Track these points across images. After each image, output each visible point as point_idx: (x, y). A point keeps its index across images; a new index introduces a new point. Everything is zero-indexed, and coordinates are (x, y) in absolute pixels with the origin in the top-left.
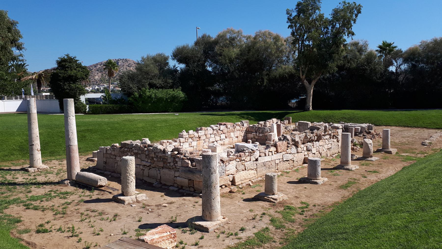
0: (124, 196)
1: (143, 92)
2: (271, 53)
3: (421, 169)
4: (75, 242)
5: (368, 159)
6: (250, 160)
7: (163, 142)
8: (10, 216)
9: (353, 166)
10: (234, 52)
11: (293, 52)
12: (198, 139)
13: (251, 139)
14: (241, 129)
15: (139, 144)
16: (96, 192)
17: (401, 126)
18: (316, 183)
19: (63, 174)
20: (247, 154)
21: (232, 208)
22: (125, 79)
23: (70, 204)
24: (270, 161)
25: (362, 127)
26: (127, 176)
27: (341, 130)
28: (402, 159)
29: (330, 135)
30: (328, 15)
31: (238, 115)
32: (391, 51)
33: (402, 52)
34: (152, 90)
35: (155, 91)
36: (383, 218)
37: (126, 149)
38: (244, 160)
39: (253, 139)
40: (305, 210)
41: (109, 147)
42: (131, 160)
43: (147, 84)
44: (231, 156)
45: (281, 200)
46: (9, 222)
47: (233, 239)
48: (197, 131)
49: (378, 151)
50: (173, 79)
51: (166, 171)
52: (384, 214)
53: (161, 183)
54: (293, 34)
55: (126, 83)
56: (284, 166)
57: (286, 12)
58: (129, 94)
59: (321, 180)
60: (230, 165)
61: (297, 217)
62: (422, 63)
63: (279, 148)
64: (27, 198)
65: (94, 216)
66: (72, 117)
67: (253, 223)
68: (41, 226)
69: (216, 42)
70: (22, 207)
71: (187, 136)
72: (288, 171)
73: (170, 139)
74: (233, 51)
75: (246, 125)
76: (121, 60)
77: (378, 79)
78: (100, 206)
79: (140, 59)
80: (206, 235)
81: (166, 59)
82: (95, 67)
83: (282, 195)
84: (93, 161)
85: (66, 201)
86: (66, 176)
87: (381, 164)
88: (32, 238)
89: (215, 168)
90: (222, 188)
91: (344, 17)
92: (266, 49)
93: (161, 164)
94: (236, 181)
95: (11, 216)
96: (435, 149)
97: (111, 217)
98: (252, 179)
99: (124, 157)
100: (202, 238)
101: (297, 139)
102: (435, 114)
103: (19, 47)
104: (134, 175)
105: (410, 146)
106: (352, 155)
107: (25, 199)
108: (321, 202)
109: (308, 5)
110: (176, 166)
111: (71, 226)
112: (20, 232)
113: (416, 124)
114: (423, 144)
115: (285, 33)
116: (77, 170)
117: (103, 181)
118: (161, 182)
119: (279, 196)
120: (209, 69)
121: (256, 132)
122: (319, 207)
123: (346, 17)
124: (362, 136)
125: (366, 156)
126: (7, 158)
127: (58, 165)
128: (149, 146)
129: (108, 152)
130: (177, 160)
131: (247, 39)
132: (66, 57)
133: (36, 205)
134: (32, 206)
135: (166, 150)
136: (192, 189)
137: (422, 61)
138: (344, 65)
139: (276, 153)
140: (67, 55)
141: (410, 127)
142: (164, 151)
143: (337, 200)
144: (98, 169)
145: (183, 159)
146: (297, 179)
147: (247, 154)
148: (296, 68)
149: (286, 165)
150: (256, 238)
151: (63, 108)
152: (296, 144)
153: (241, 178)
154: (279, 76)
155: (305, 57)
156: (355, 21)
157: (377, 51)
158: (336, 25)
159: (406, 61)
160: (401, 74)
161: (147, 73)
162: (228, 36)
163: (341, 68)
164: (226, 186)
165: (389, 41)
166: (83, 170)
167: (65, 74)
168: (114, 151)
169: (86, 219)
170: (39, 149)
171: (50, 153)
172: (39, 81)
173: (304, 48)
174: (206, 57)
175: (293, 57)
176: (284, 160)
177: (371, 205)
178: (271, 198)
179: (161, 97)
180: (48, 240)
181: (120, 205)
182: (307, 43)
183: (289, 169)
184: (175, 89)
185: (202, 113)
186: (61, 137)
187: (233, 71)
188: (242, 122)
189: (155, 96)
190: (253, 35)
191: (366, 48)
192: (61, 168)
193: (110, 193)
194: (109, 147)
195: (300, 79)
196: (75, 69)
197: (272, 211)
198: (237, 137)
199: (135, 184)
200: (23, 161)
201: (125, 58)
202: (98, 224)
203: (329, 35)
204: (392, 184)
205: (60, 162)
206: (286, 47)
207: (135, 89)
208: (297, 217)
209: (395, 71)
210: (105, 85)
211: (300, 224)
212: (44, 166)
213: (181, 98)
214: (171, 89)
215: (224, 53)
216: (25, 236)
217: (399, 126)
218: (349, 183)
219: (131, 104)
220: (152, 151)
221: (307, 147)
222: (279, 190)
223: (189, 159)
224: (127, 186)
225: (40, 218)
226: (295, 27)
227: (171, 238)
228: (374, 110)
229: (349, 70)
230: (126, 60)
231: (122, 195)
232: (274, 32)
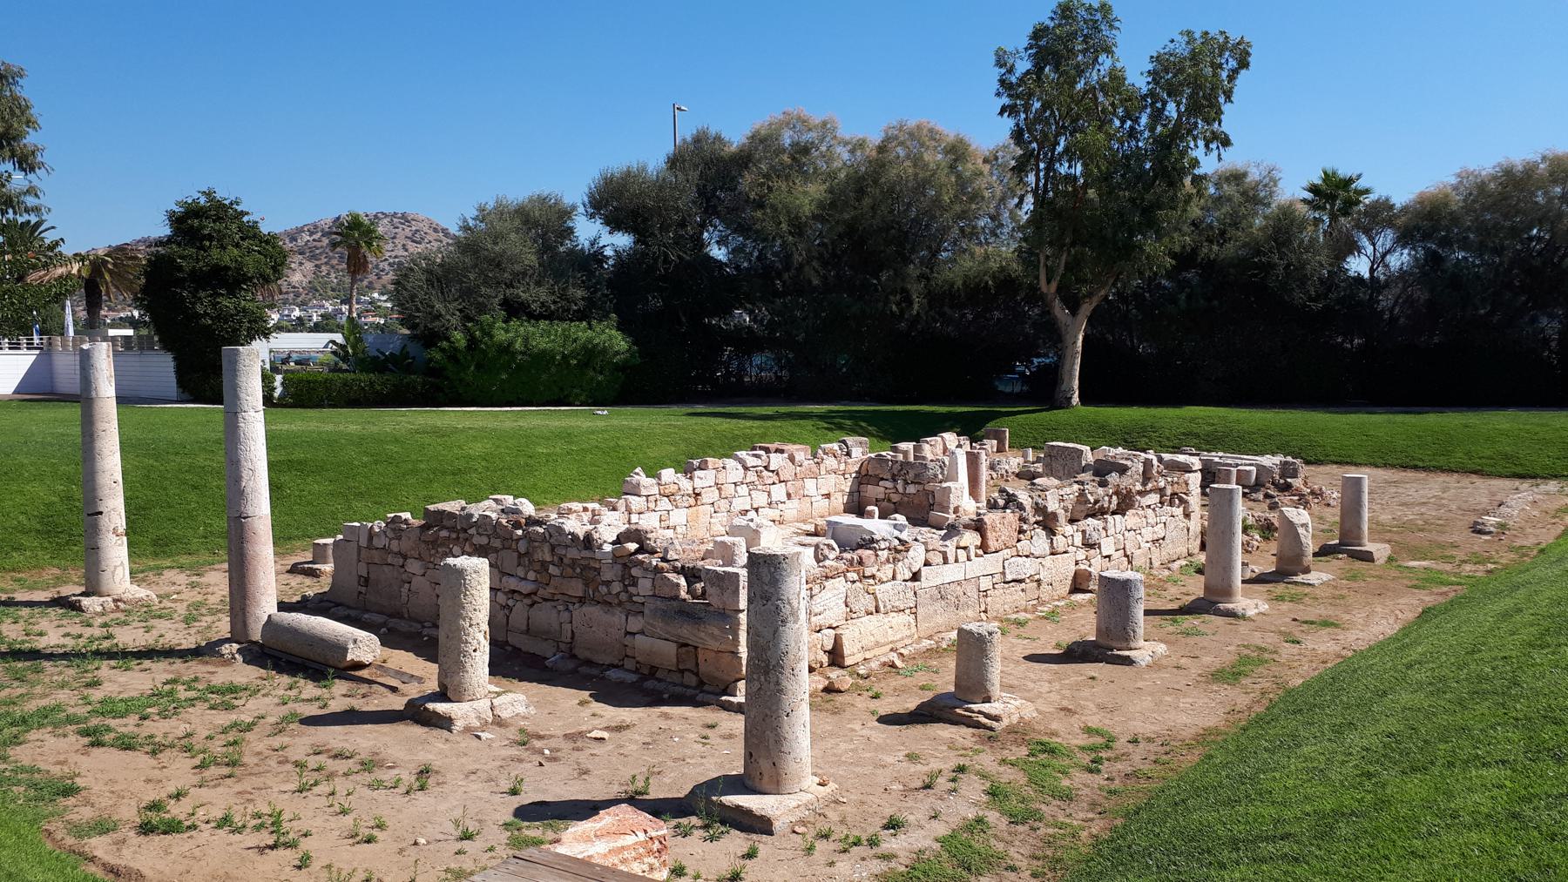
0: (449, 700)
1: (482, 330)
2: (937, 201)
3: (1506, 615)
4: (288, 869)
5: (1295, 579)
6: (894, 578)
8: (33, 770)
9: (1248, 602)
10: (808, 195)
11: (1016, 200)
12: (692, 501)
13: (877, 502)
14: (842, 467)
15: (494, 516)
16: (340, 687)
17: (1393, 466)
18: (1128, 661)
19: (209, 619)
20: (884, 554)
21: (843, 746)
23: (249, 727)
24: (959, 583)
25: (1261, 468)
26: (460, 629)
27: (1199, 475)
28: (1410, 579)
29: (1161, 491)
30: (1138, 79)
31: (821, 417)
32: (1350, 203)
33: (1392, 207)
34: (514, 323)
35: (527, 328)
36: (1416, 787)
38: (873, 577)
39: (885, 504)
40: (1103, 755)
41: (378, 526)
42: (477, 570)
44: (827, 563)
45: (1015, 719)
46: (32, 793)
47: (863, 859)
48: (688, 471)
49: (1324, 552)
50: (588, 288)
51: (593, 611)
52: (1414, 770)
53: (574, 656)
54: (1017, 136)
55: (421, 295)
56: (1009, 599)
57: (994, 58)
58: (429, 338)
59: (1144, 650)
60: (826, 594)
61: (1078, 780)
62: (1461, 248)
63: (990, 535)
64: (89, 708)
65: (345, 774)
66: (252, 413)
67: (926, 802)
68: (155, 806)
69: (743, 160)
70: (74, 741)
71: (655, 490)
72: (1022, 616)
73: (593, 501)
74: (805, 193)
75: (858, 454)
76: (386, 216)
77: (1311, 299)
78: (363, 738)
79: (471, 213)
80: (764, 844)
81: (566, 214)
82: (293, 239)
83: (1017, 703)
84: (313, 573)
85: (233, 717)
86: (223, 627)
87: (1343, 597)
88: (124, 851)
89: (795, 603)
91: (1196, 83)
92: (922, 185)
93: (576, 588)
94: (846, 652)
95: (39, 771)
96: (1522, 547)
97: (408, 777)
98: (899, 645)
99: (450, 561)
100: (750, 855)
101: (1052, 505)
102: (1506, 426)
103: (26, 162)
104: (485, 627)
105: (1434, 536)
106: (1243, 564)
107: (82, 711)
109: (1072, 36)
110: (631, 595)
111: (266, 810)
112: (80, 831)
113: (1442, 461)
114: (1478, 530)
115: (989, 131)
116: (266, 606)
117: (364, 645)
118: (576, 651)
119: (1005, 706)
120: (718, 253)
121: (895, 480)
122: (1152, 747)
123: (1199, 81)
124: (1261, 497)
125: (1287, 569)
127: (189, 597)
128: (531, 521)
129: (375, 542)
130: (634, 572)
131: (852, 152)
132: (203, 200)
133: (122, 730)
134: (112, 735)
135: (596, 536)
136: (691, 680)
137: (1465, 245)
138: (1195, 251)
139: (980, 552)
141: (1425, 469)
142: (588, 542)
143: (1211, 721)
144: (337, 605)
145: (657, 570)
146: (1058, 645)
147: (884, 554)
148: (1027, 256)
149: (1015, 595)
150: (945, 855)
152: (1048, 523)
153: (864, 643)
155: (1058, 218)
156: (1228, 95)
157: (1304, 201)
158: (1164, 108)
159: (1405, 238)
160: (1387, 285)
161: (497, 263)
162: (787, 139)
163: (1185, 259)
165: (1344, 172)
166: (283, 606)
167: (198, 260)
168: (399, 538)
169: (316, 784)
171: (155, 543)
172: (95, 282)
173: (1055, 187)
174: (706, 211)
175: (1013, 217)
176: (1009, 578)
177: (1352, 737)
179: (544, 351)
180: (186, 861)
181: (437, 732)
182: (1063, 169)
183: (1025, 611)
184: (594, 322)
185: (690, 410)
186: (195, 487)
187: (801, 266)
188: (844, 442)
190: (875, 138)
191: (1271, 193)
192: (200, 598)
193: (394, 690)
194: (378, 526)
195: (1034, 296)
196: (237, 246)
197: (987, 760)
198: (828, 496)
199: (487, 658)
200: (56, 571)
201: (400, 211)
202: (368, 804)
204: (1409, 666)
205: (194, 578)
206: (991, 183)
208: (1078, 780)
209: (1367, 276)
210: (327, 304)
211: (1093, 805)
212: (141, 592)
213: (617, 353)
214: (580, 320)
215: (772, 199)
216: (99, 846)
217: (1385, 466)
218: (1244, 660)
219: (433, 371)
220: (543, 539)
221: (1084, 532)
222: (1004, 687)
224: (460, 667)
225: (148, 781)
226: (1026, 112)
227: (650, 852)
229: (1210, 266)
230: (404, 216)
231: (442, 696)
232: (950, 130)
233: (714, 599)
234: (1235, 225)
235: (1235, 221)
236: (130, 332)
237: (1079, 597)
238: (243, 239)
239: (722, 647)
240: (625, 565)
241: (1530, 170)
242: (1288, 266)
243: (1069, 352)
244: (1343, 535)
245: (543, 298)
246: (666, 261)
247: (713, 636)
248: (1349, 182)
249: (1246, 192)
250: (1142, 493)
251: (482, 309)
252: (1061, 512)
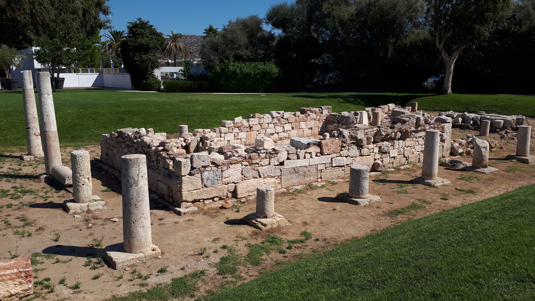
1: (225, 66)
6: (269, 164)
7: (197, 132)
12: (248, 129)
14: (318, 117)
18: (356, 203)
24: (306, 167)
25: (506, 121)
56: (334, 173)
58: (210, 68)
66: (46, 95)
71: (232, 125)
75: (326, 112)
81: (259, 22)
89: (136, 179)
94: (238, 193)
103: (106, 12)
108: (334, 234)
110: (158, 167)
126: (19, 141)
132: (138, 22)
138: (509, 29)
139: (319, 154)
140: (140, 19)
145: (164, 158)
152: (359, 144)
154: (411, 44)
161: (233, 41)
164: (221, 199)
171: (72, 138)
176: (334, 165)
178: (260, 222)
185: (309, 94)
186: (94, 119)
189: (241, 71)
198: (311, 128)
207: (217, 62)
213: (274, 74)
228: (519, 94)
243: (447, 72)
244: (518, 152)
245: (248, 54)
246: (293, 38)
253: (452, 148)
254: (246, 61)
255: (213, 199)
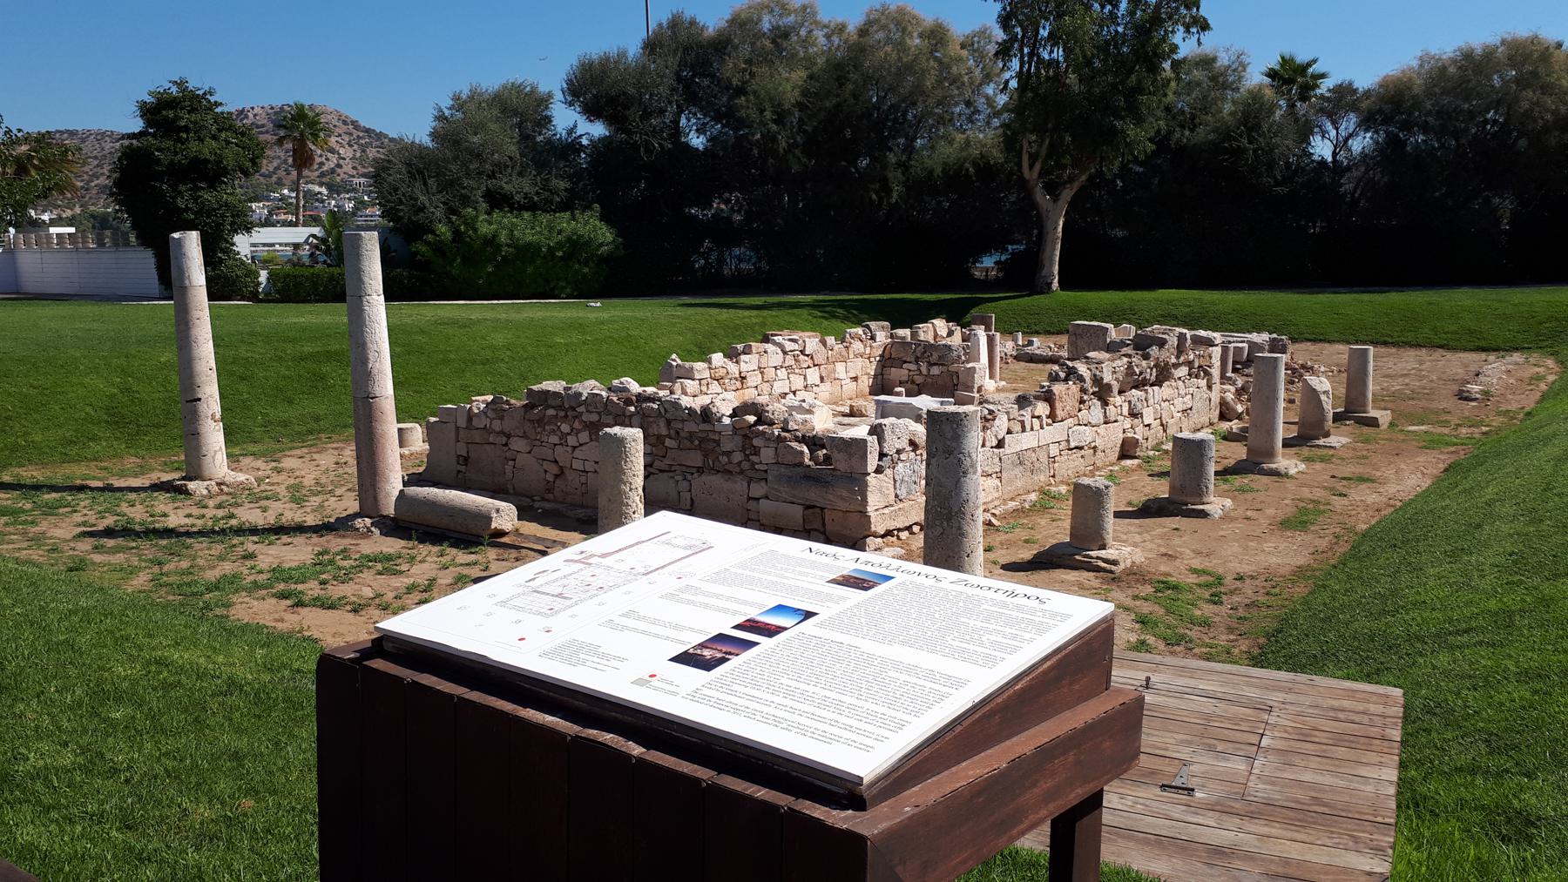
10: (789, 82)
12: (738, 384)
18: (1203, 514)
22: (396, 176)
24: (1034, 450)
25: (1252, 345)
26: (621, 493)
29: (1190, 364)
32: (1306, 91)
35: (509, 219)
37: (551, 412)
42: (634, 436)
43: (479, 193)
48: (733, 355)
51: (715, 480)
59: (1216, 504)
63: (1058, 405)
69: (721, 45)
71: (707, 374)
75: (882, 337)
77: (1278, 184)
81: (544, 101)
86: (354, 507)
90: (912, 533)
93: (695, 459)
102: (1468, 302)
110: (753, 464)
113: (1410, 337)
114: (1464, 397)
116: (393, 483)
120: (697, 141)
121: (917, 360)
126: (73, 451)
127: (319, 472)
129: (475, 422)
130: (756, 442)
131: (828, 36)
132: (174, 89)
137: (1425, 129)
141: (1394, 344)
142: (706, 414)
143: (1302, 561)
145: (780, 439)
148: (1010, 141)
151: (169, 280)
152: (1103, 393)
155: (1038, 102)
159: (1367, 122)
160: (1349, 168)
165: (1302, 57)
167: (176, 154)
168: (502, 418)
170: (218, 416)
176: (1073, 445)
179: (529, 244)
186: (243, 379)
188: (868, 327)
190: (854, 21)
191: (1240, 78)
196: (214, 138)
198: (855, 379)
203: (1120, 29)
207: (439, 213)
209: (1330, 159)
213: (602, 245)
215: (754, 85)
220: (659, 413)
223: (803, 440)
233: (841, 463)
234: (1205, 111)
235: (1205, 105)
236: (72, 230)
237: (1128, 463)
238: (220, 131)
239: (852, 507)
240: (745, 436)
241: (1489, 54)
242: (1255, 151)
245: (526, 189)
246: (648, 151)
247: (842, 498)
248: (1303, 68)
249: (1217, 77)
250: (1176, 366)
251: (466, 201)
252: (1114, 383)
253: (1223, 403)
254: (522, 208)
255: (909, 528)
